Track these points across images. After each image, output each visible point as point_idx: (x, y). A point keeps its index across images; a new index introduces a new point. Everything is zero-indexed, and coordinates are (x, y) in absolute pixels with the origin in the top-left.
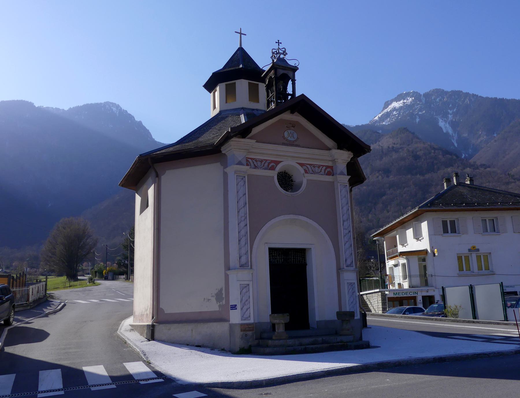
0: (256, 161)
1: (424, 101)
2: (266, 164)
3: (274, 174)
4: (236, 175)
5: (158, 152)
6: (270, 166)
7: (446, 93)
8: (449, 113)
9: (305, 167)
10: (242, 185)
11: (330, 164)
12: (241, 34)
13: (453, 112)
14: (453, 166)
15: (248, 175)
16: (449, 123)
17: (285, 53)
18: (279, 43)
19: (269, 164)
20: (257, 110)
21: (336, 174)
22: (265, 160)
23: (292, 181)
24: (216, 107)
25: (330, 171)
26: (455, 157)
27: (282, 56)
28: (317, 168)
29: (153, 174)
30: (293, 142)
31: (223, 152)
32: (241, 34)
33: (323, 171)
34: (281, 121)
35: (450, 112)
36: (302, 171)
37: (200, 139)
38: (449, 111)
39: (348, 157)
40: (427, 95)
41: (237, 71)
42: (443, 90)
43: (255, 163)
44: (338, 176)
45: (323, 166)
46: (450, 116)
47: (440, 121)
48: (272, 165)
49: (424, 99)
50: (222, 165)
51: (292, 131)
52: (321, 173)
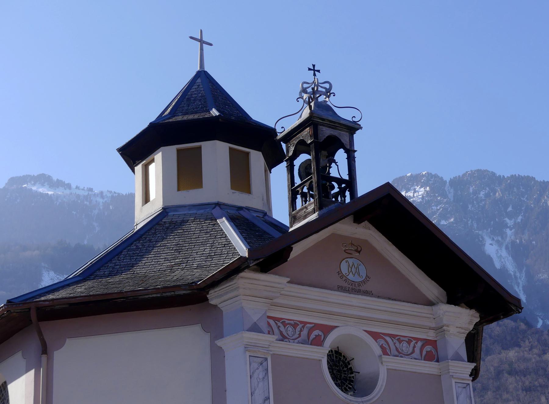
0: (284, 324)
1: (451, 196)
2: (305, 332)
3: (320, 354)
4: (248, 354)
5: (51, 297)
6: (312, 336)
7: (500, 180)
8: (506, 226)
9: (382, 342)
10: (261, 377)
11: (431, 335)
12: (202, 42)
13: (515, 223)
14: (520, 346)
15: (273, 355)
16: (507, 248)
17: (328, 92)
18: (314, 70)
19: (310, 331)
20: (248, 209)
21: (446, 358)
22: (301, 322)
23: (351, 371)
24: (153, 195)
25: (432, 352)
26: (523, 326)
27: (322, 99)
28: (405, 344)
29: (34, 344)
30: (359, 285)
31: (212, 302)
32: (202, 42)
33: (417, 350)
34: (333, 237)
35: (510, 222)
36: (378, 351)
37: (140, 269)
38: (507, 220)
39: (470, 323)
40: (458, 183)
41: (198, 123)
42: (493, 174)
43: (282, 328)
44: (451, 363)
45: (417, 339)
46: (509, 232)
47: (488, 241)
48: (317, 334)
49: (452, 190)
50: (205, 329)
51: (356, 262)
52: (413, 355)
